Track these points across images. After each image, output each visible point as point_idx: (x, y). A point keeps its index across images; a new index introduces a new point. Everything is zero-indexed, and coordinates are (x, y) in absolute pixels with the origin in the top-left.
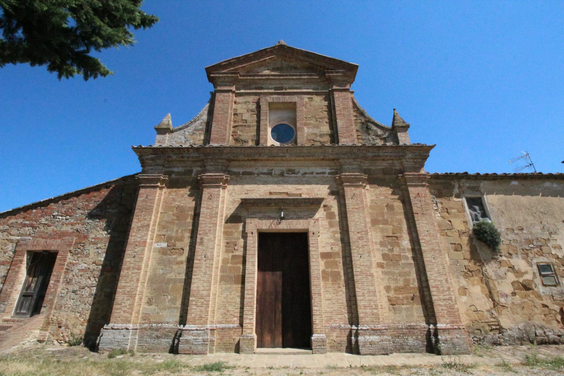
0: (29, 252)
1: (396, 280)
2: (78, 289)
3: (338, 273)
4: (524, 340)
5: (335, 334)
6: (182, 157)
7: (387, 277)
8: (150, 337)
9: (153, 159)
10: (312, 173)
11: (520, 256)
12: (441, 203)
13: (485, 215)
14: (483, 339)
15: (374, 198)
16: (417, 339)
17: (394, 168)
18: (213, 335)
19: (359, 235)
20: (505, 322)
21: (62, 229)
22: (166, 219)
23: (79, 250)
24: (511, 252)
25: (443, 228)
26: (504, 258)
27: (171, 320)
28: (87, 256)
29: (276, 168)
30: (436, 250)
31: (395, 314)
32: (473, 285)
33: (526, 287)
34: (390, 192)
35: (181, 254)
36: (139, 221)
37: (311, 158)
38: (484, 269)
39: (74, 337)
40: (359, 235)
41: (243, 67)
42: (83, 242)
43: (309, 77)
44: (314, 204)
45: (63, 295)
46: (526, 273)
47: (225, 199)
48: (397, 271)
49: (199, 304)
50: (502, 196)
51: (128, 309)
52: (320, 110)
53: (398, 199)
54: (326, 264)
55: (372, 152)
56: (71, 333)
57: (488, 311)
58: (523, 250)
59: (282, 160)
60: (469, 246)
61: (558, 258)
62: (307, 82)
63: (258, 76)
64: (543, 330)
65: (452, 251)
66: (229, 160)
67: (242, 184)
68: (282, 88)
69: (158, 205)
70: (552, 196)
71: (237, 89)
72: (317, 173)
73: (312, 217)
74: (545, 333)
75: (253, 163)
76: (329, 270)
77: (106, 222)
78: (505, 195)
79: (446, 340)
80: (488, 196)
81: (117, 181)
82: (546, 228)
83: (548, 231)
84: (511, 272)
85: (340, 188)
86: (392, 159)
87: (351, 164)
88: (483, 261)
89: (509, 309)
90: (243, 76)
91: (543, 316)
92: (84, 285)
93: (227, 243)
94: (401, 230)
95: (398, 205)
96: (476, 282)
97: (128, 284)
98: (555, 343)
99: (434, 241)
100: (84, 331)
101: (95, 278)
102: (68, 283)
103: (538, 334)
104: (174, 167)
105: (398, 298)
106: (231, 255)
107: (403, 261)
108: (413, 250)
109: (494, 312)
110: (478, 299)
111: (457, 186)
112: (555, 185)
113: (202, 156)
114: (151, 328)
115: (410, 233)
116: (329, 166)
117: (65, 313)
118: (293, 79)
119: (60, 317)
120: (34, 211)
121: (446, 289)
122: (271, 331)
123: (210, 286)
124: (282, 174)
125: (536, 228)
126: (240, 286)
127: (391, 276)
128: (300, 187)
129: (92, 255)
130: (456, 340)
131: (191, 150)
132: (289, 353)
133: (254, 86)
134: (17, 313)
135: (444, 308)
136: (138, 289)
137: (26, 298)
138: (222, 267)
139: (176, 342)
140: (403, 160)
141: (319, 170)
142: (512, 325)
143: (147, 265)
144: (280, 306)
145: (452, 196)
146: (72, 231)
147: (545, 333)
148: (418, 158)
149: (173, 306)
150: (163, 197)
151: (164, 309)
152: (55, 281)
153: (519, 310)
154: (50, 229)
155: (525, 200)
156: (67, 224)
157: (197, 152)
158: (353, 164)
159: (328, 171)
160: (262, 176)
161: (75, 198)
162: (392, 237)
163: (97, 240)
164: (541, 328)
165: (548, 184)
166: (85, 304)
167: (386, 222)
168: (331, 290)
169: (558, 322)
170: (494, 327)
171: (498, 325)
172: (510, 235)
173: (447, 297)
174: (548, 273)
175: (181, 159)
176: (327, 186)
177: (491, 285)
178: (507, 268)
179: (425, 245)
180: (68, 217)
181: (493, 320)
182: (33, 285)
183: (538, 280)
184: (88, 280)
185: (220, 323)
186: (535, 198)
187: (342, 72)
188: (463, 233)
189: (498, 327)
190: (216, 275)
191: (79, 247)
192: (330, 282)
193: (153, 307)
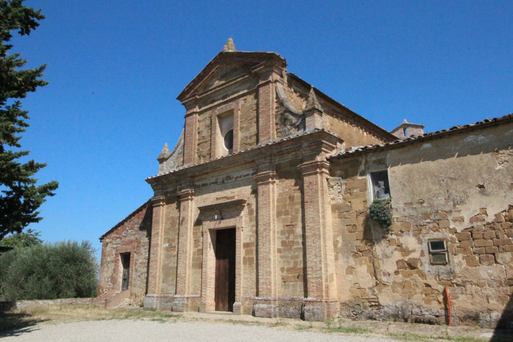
0: (120, 254)
1: (288, 262)
3: (253, 258)
4: (399, 318)
5: (247, 303)
7: (283, 260)
8: (164, 301)
10: (241, 177)
11: (411, 234)
12: (346, 184)
13: (387, 190)
14: (361, 313)
15: (281, 192)
16: (295, 308)
17: (298, 158)
18: (188, 301)
19: (264, 227)
20: (384, 300)
22: (167, 227)
24: (403, 230)
25: (342, 211)
26: (394, 237)
28: (142, 254)
29: (219, 177)
30: (316, 235)
31: (285, 289)
32: (361, 264)
33: (412, 266)
34: (293, 184)
35: (175, 250)
36: (155, 230)
38: (374, 248)
40: (264, 227)
41: (200, 86)
43: (242, 78)
44: (237, 206)
46: (414, 251)
47: (192, 207)
48: (290, 255)
50: (408, 166)
52: (251, 111)
53: (299, 189)
54: (246, 252)
55: (276, 149)
57: (370, 288)
58: (417, 226)
60: (363, 226)
61: (456, 232)
62: (243, 83)
64: (421, 309)
65: (346, 232)
66: (193, 177)
67: (202, 194)
69: (162, 218)
70: (472, 154)
71: (200, 108)
72: (245, 176)
73: (238, 216)
74: (421, 312)
75: (205, 176)
76: (247, 256)
78: (412, 163)
79: (309, 310)
80: (395, 168)
82: (451, 197)
83: (453, 201)
84: (399, 251)
86: (295, 151)
87: (263, 163)
88: (374, 241)
89: (390, 288)
90: (201, 95)
91: (424, 296)
93: (195, 241)
94: (297, 218)
95: (298, 194)
96: (363, 262)
98: (430, 322)
99: (317, 227)
103: (413, 312)
105: (288, 277)
106: (197, 249)
107: (295, 246)
109: (375, 290)
110: (362, 277)
111: (364, 161)
112: (481, 138)
116: (252, 167)
118: (232, 84)
121: (318, 269)
122: (223, 301)
123: (186, 270)
125: (440, 198)
127: (285, 260)
130: (316, 310)
131: (171, 175)
134: (123, 290)
135: (315, 285)
136: (158, 274)
138: (193, 257)
140: (301, 150)
141: (246, 172)
142: (390, 303)
143: (160, 259)
144: (227, 284)
145: (356, 175)
147: (421, 312)
148: (313, 146)
150: (165, 212)
151: (169, 285)
153: (399, 289)
155: (432, 165)
158: (265, 163)
160: (212, 185)
161: (133, 217)
162: (290, 225)
164: (419, 307)
165: (470, 138)
167: (287, 213)
168: (247, 271)
169: (440, 303)
170: (373, 304)
171: (378, 302)
172: (407, 211)
173: (318, 276)
174: (439, 250)
176: (250, 187)
177: (376, 264)
178: (395, 247)
179: (309, 231)
181: (373, 297)
183: (426, 259)
185: (192, 294)
186: (448, 160)
187: (264, 64)
188: (361, 213)
189: (377, 304)
190: (189, 263)
192: (248, 266)
193: (165, 284)
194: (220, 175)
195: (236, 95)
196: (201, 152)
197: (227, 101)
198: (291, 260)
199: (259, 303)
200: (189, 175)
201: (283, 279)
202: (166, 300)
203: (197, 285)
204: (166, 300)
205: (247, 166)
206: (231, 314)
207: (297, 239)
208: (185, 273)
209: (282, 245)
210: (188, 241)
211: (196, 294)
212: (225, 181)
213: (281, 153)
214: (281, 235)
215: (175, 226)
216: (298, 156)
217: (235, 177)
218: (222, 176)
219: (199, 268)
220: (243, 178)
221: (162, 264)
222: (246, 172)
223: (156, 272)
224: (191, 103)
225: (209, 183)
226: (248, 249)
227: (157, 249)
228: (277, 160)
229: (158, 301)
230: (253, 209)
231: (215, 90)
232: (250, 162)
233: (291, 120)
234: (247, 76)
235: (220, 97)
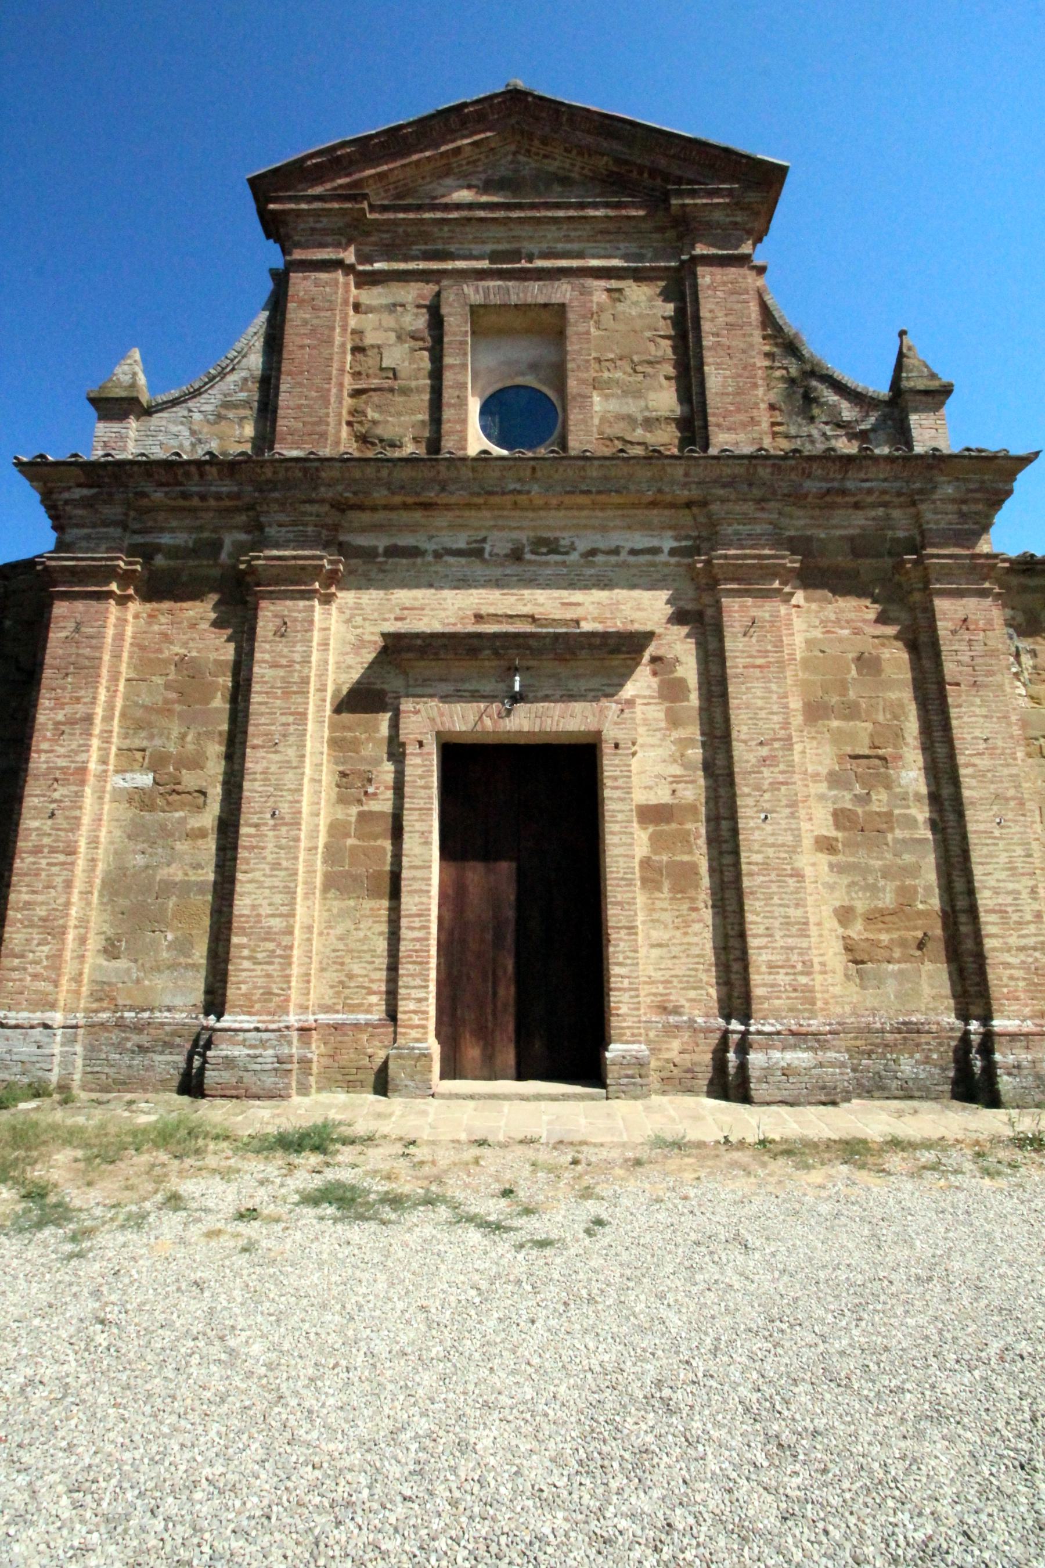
1: (874, 889)
3: (693, 868)
5: (676, 1045)
6: (185, 496)
7: (845, 880)
10: (616, 551)
12: (1034, 654)
16: (927, 1060)
18: (306, 1043)
27: (178, 1001)
30: (1007, 799)
34: (872, 615)
36: (60, 705)
37: (615, 498)
40: (764, 751)
41: (381, 176)
43: (611, 213)
47: (332, 634)
52: (648, 334)
53: (896, 638)
55: (824, 479)
63: (446, 207)
66: (341, 507)
67: (385, 585)
68: (515, 255)
71: (362, 258)
72: (633, 552)
75: (418, 515)
85: (707, 599)
93: (343, 775)
97: (40, 898)
99: (1006, 771)
104: (162, 530)
105: (875, 943)
106: (354, 810)
107: (898, 833)
114: (120, 1025)
115: (927, 748)
118: (555, 220)
121: (1029, 917)
122: (485, 1036)
123: (292, 903)
124: (516, 555)
126: (385, 903)
133: (416, 249)
136: (73, 911)
138: (327, 846)
139: (978, 1064)
141: (641, 541)
148: (976, 501)
149: (182, 960)
150: (129, 631)
151: (157, 969)
158: (754, 520)
167: (851, 712)
168: (667, 917)
176: (664, 595)
179: (973, 782)
185: (328, 1009)
187: (730, 192)
190: (311, 872)
192: (666, 893)
193: (122, 964)
194: (502, 528)
195: (575, 263)
196: (374, 422)
197: (514, 270)
198: (882, 883)
199: (768, 1047)
201: (848, 949)
206: (592, 1098)
207: (908, 807)
208: (292, 915)
209: (838, 826)
210: (308, 770)
212: (528, 556)
213: (830, 499)
214: (830, 788)
215: (207, 700)
216: (893, 529)
217: (582, 546)
218: (515, 535)
219: (373, 893)
221: (101, 866)
223: (68, 904)
225: (430, 546)
226: (665, 827)
227: (79, 795)
228: (798, 523)
229: (79, 1048)
230: (682, 682)
231: (465, 213)
232: (672, 506)
233: (834, 409)
234: (641, 213)
235: (489, 248)
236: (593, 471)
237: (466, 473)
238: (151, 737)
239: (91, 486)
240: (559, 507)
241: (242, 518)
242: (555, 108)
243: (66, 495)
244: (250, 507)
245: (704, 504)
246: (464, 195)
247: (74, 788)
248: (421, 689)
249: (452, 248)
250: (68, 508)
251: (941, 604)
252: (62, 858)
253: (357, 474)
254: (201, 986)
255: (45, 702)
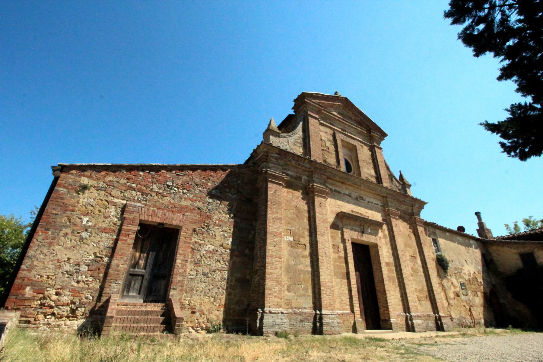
2: (208, 271)
6: (299, 165)
8: (296, 320)
9: (276, 159)
10: (372, 203)
21: (180, 203)
23: (204, 230)
27: (306, 306)
37: (374, 192)
39: (211, 323)
42: (206, 222)
45: (192, 277)
47: (329, 208)
49: (328, 293)
51: (278, 294)
56: (208, 319)
59: (357, 188)
63: (331, 113)
68: (345, 131)
72: (375, 204)
75: (340, 184)
77: (229, 205)
81: (232, 166)
85: (388, 217)
92: (215, 268)
97: (274, 271)
100: (221, 317)
101: (224, 261)
102: (196, 264)
104: (289, 170)
108: (423, 266)
113: (312, 169)
114: (295, 313)
115: (420, 256)
117: (198, 297)
119: (192, 302)
120: (141, 173)
124: (356, 199)
126: (346, 281)
128: (367, 211)
129: (218, 238)
132: (383, 333)
133: (328, 121)
137: (135, 278)
139: (318, 324)
141: (376, 202)
146: (192, 207)
149: (306, 294)
152: (182, 260)
154: (166, 200)
156: (186, 199)
157: (310, 163)
159: (380, 204)
163: (221, 223)
166: (218, 288)
175: (297, 166)
180: (185, 191)
182: (142, 262)
184: (218, 263)
191: (204, 226)
193: (292, 294)
200: (327, 174)
202: (300, 318)
203: (343, 298)
204: (300, 318)
205: (378, 197)
211: (344, 309)
215: (303, 220)
219: (343, 278)
220: (373, 205)
222: (375, 202)
224: (314, 108)
235: (340, 127)
236: (372, 186)
237: (407, 200)
238: (292, 227)
239: (278, 154)
240: (364, 191)
241: (307, 173)
242: (353, 105)
243: (272, 155)
244: (312, 172)
245: (386, 197)
246: (335, 113)
247: (279, 239)
248: (347, 226)
249: (334, 124)
250: (271, 158)
251: (270, 185)
252: (278, 259)
253: (334, 172)
254: (311, 301)
255: (269, 211)
